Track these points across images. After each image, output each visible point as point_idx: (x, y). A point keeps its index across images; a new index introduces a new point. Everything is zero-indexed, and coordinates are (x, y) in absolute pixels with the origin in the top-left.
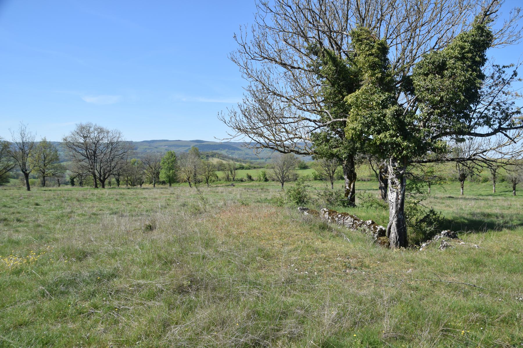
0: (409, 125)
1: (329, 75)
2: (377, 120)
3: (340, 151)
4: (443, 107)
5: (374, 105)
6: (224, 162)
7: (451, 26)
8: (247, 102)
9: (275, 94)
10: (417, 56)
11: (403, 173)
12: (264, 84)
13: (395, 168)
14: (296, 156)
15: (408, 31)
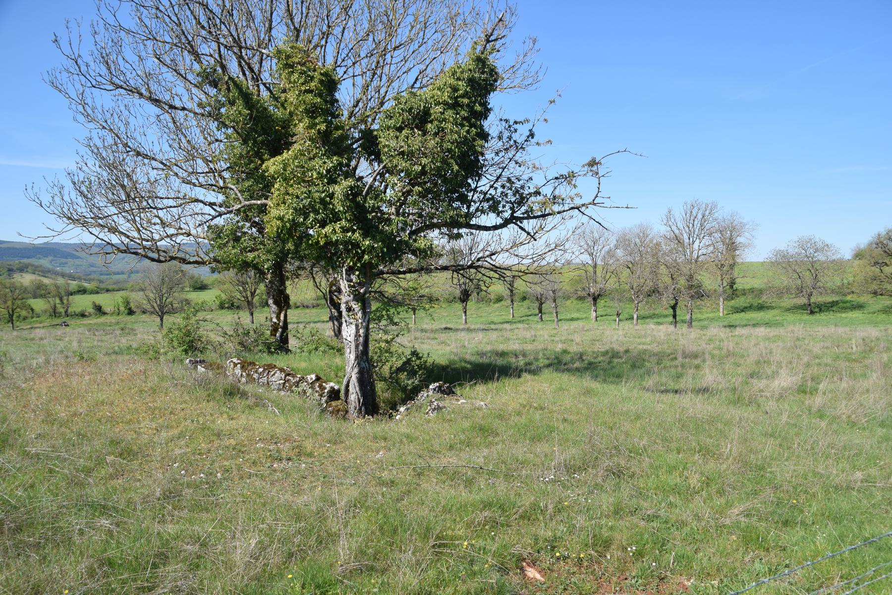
0: (373, 211)
1: (237, 123)
2: (320, 203)
3: (259, 257)
5: (314, 177)
6: (46, 281)
7: (439, 53)
8: (85, 168)
9: (138, 154)
11: (365, 293)
13: (352, 284)
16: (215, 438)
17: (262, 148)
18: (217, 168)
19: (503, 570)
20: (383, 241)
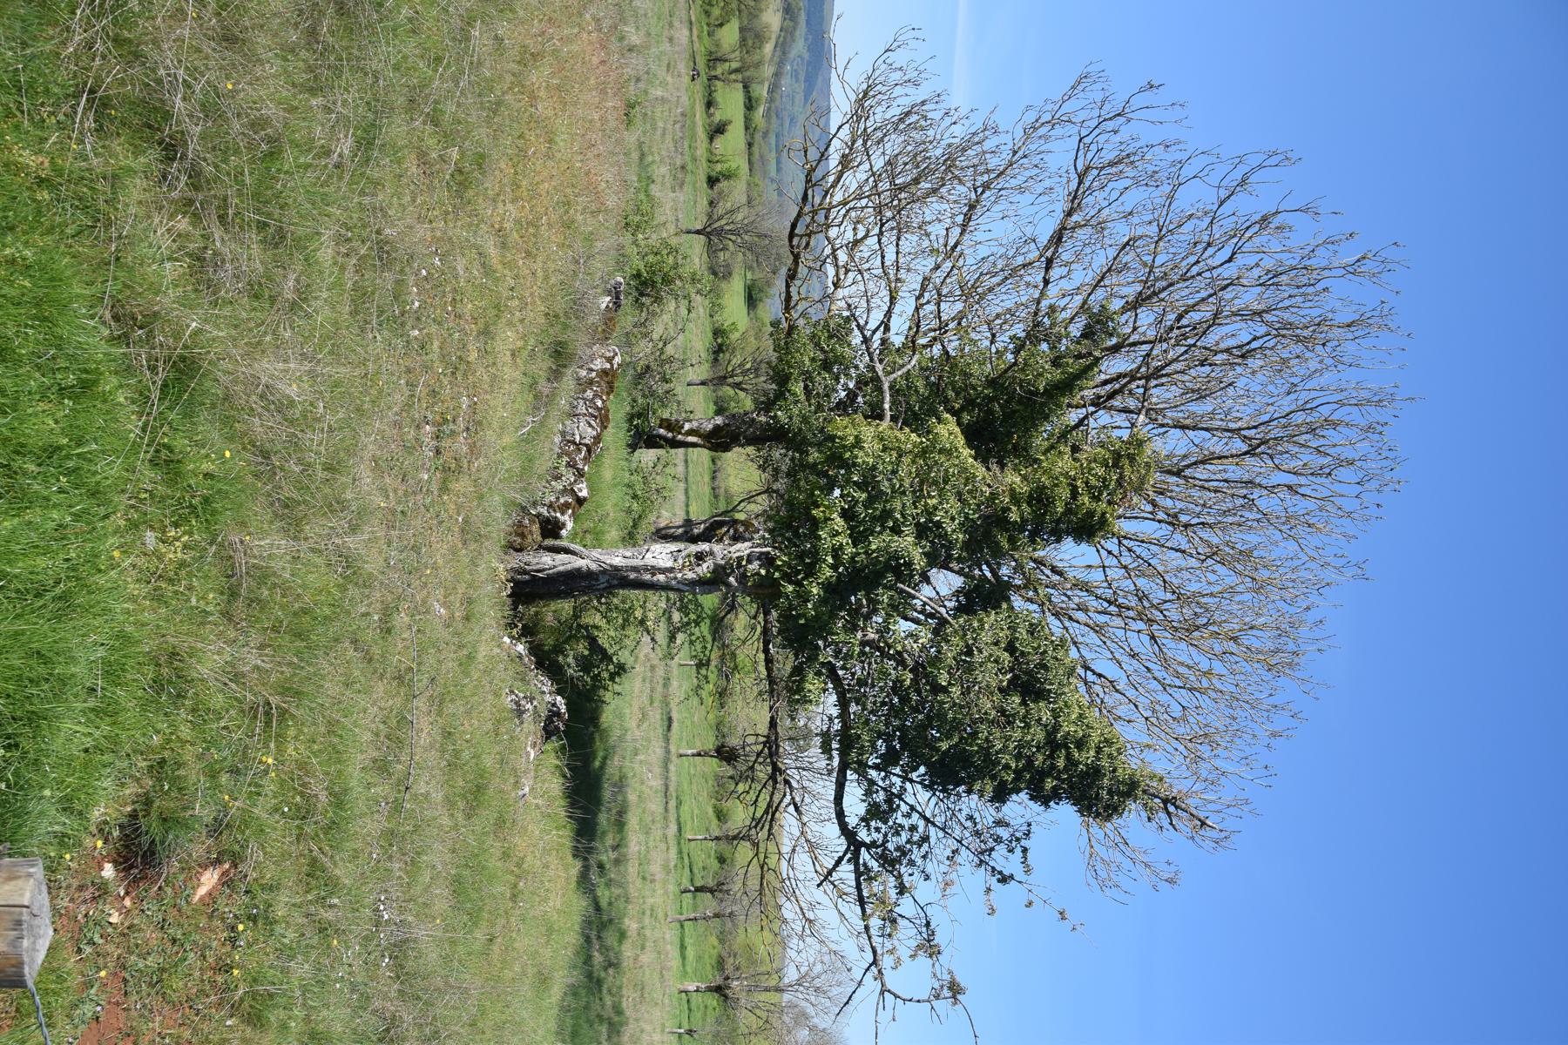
0: (870, 601)
1: (1023, 370)
2: (884, 511)
4: (919, 694)
6: (768, 48)
7: (1148, 714)
8: (948, 121)
10: (1067, 624)
11: (728, 585)
12: (1002, 173)
14: (784, 271)
15: (1140, 600)
16: (481, 326)
17: (980, 410)
18: (948, 334)
19: (217, 828)
20: (817, 618)
